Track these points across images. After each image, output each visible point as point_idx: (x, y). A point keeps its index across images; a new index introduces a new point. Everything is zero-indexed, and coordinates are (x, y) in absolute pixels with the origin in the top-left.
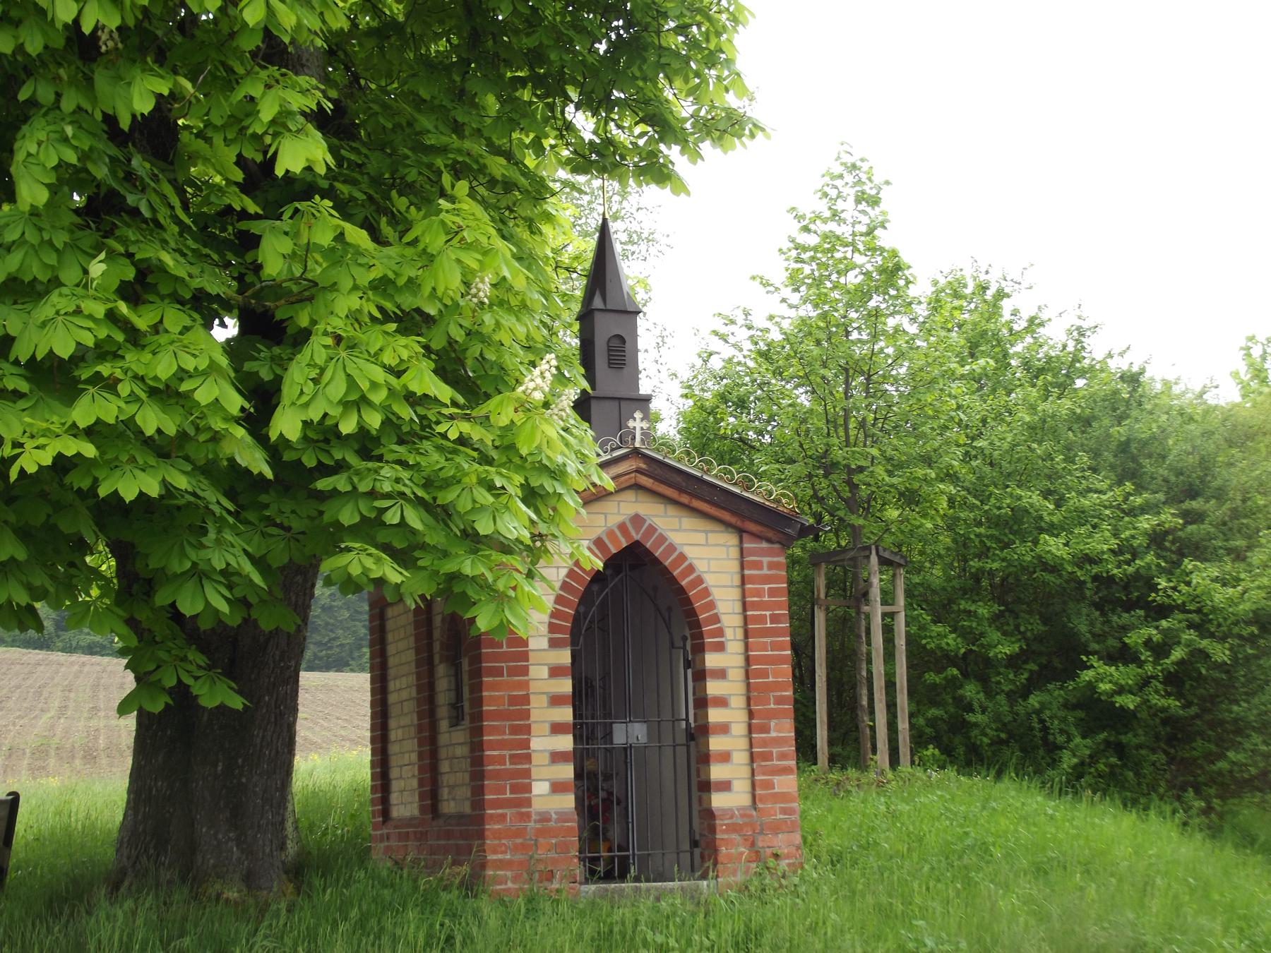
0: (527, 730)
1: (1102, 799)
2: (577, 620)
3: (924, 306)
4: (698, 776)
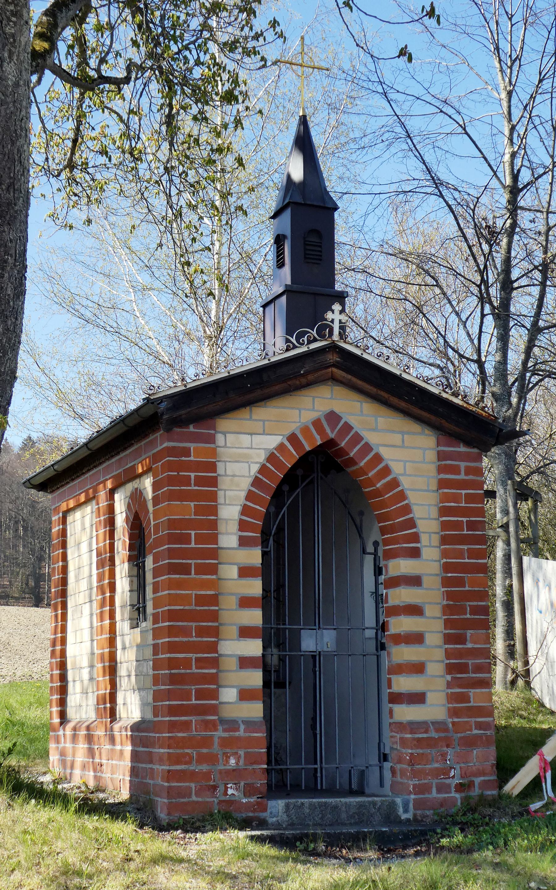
0: (215, 632)
1: (45, 806)
2: (268, 518)
3: (99, 761)
4: (390, 687)
